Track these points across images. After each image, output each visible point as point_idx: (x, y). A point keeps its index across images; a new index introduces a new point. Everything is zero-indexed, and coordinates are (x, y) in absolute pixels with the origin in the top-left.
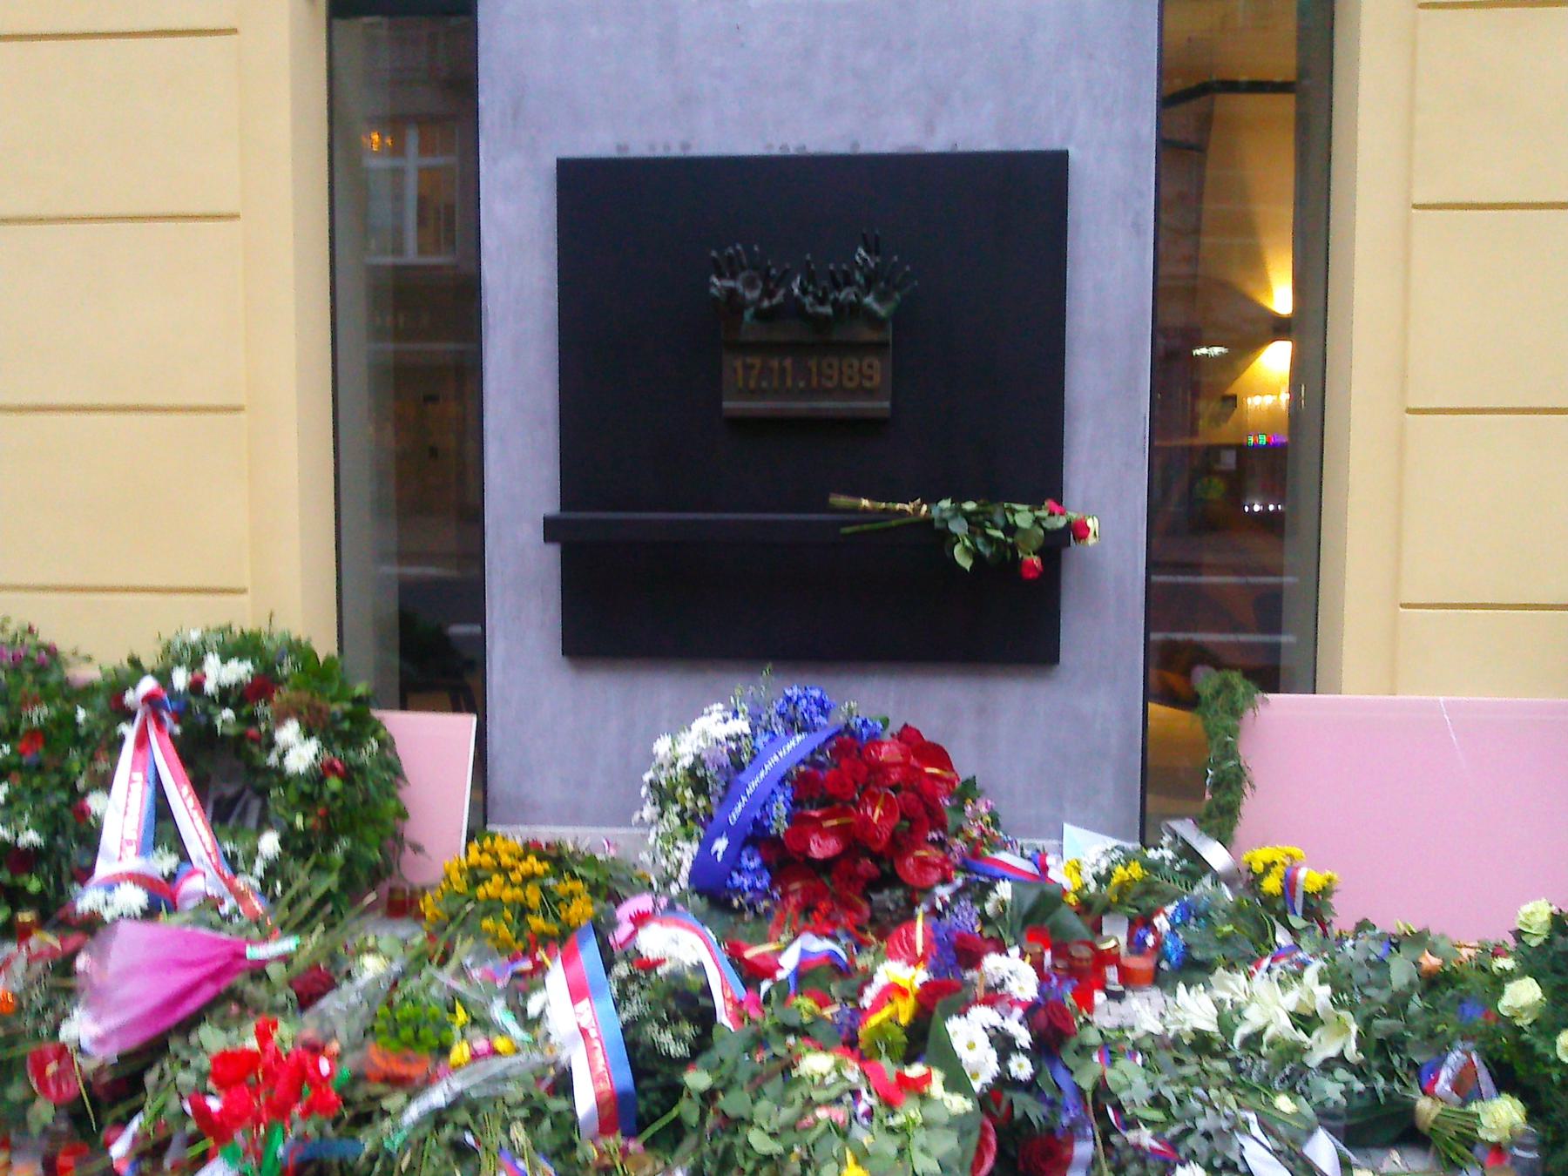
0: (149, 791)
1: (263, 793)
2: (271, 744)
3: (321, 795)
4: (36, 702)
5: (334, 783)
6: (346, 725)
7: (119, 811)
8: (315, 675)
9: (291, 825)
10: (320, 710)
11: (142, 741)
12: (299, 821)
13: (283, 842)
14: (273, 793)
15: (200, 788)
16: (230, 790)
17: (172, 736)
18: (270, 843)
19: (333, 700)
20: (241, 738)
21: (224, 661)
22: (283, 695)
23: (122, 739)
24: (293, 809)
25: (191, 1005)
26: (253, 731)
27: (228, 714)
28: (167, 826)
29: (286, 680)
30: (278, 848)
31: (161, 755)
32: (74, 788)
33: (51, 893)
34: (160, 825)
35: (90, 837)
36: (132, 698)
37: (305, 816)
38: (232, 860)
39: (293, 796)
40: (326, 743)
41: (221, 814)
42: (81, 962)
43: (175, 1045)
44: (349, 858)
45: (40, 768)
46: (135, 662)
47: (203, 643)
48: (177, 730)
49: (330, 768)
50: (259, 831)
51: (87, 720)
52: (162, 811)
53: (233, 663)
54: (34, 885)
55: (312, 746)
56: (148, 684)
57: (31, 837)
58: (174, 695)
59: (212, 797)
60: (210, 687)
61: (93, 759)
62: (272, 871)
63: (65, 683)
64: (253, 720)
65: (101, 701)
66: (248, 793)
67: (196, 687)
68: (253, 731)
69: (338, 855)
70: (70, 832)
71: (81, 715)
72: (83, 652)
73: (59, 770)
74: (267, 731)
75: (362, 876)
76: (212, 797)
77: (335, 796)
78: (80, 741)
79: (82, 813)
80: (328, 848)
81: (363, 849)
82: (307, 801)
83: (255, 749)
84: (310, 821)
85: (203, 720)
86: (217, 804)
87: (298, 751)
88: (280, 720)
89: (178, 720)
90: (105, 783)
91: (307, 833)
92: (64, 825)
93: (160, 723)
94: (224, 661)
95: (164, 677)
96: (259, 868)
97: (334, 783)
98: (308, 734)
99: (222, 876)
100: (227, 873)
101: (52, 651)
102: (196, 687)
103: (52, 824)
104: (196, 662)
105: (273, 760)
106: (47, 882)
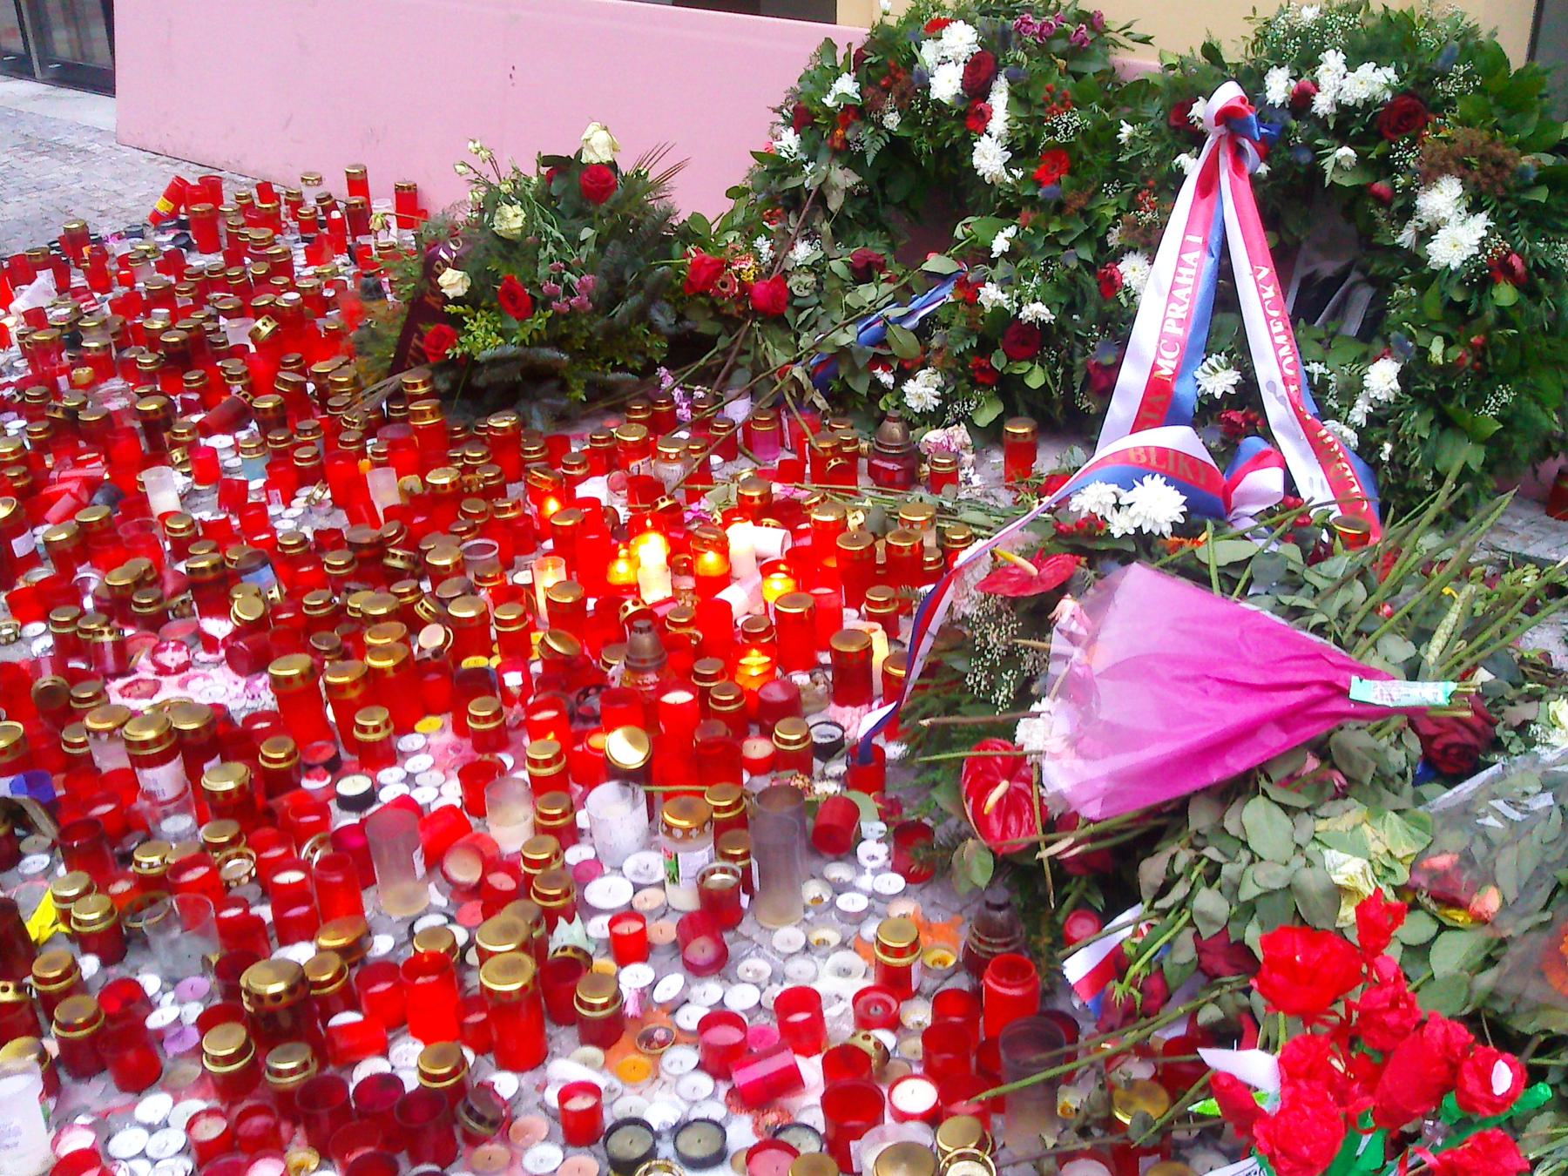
0: (1209, 263)
1: (1383, 286)
2: (1408, 212)
3: (1479, 313)
4: (1066, 104)
5: (1505, 294)
6: (1541, 195)
7: (1161, 291)
8: (1499, 99)
9: (1424, 352)
10: (1500, 165)
11: (1208, 184)
12: (1437, 349)
13: (1403, 377)
14: (1400, 292)
15: (1283, 259)
16: (1328, 268)
17: (1254, 180)
18: (1383, 378)
19: (1524, 147)
20: (1359, 191)
21: (1351, 66)
22: (1445, 130)
23: (1179, 177)
24: (1430, 328)
25: (1236, 763)
26: (1382, 186)
27: (1346, 152)
28: (1227, 319)
29: (1449, 102)
30: (1396, 386)
31: (1234, 209)
32: (1102, 245)
33: (1056, 392)
34: (1219, 317)
35: (1117, 322)
36: (1203, 111)
37: (1449, 342)
38: (1318, 389)
39: (1433, 307)
40: (1503, 224)
41: (1308, 306)
42: (1067, 607)
43: (1200, 818)
44: (1508, 420)
45: (1060, 208)
46: (1211, 52)
47: (1321, 25)
48: (1263, 169)
49: (1502, 268)
50: (1368, 359)
51: (1132, 138)
52: (1224, 297)
53: (1366, 69)
54: (1036, 379)
55: (1479, 224)
56: (1229, 93)
57: (1036, 311)
58: (1266, 112)
59: (1301, 271)
60: (1322, 104)
61: (1134, 205)
62: (1381, 417)
63: (1110, 73)
64: (1385, 167)
65: (1154, 109)
66: (1354, 276)
67: (1301, 102)
68: (1382, 186)
69: (1488, 418)
70: (1091, 309)
71: (1126, 130)
72: (1137, 30)
73: (1085, 214)
74: (1405, 188)
75: (1523, 449)
76: (1301, 271)
77: (1504, 318)
78: (1117, 172)
79: (1111, 284)
80: (1476, 401)
81: (1533, 408)
82: (1458, 317)
83: (1380, 214)
84: (1456, 353)
85: (1305, 157)
86: (1306, 282)
87: (1454, 230)
88: (1429, 178)
89: (1264, 157)
90: (1149, 243)
91: (1446, 370)
92: (1084, 301)
93: (1238, 154)
94: (1351, 66)
95: (1252, 79)
96: (1359, 414)
97: (1505, 294)
98: (1474, 208)
99: (1300, 416)
100: (1310, 409)
101: (1093, 21)
102: (1301, 102)
103: (1069, 297)
104: (1307, 62)
105: (1406, 237)
106: (1054, 377)
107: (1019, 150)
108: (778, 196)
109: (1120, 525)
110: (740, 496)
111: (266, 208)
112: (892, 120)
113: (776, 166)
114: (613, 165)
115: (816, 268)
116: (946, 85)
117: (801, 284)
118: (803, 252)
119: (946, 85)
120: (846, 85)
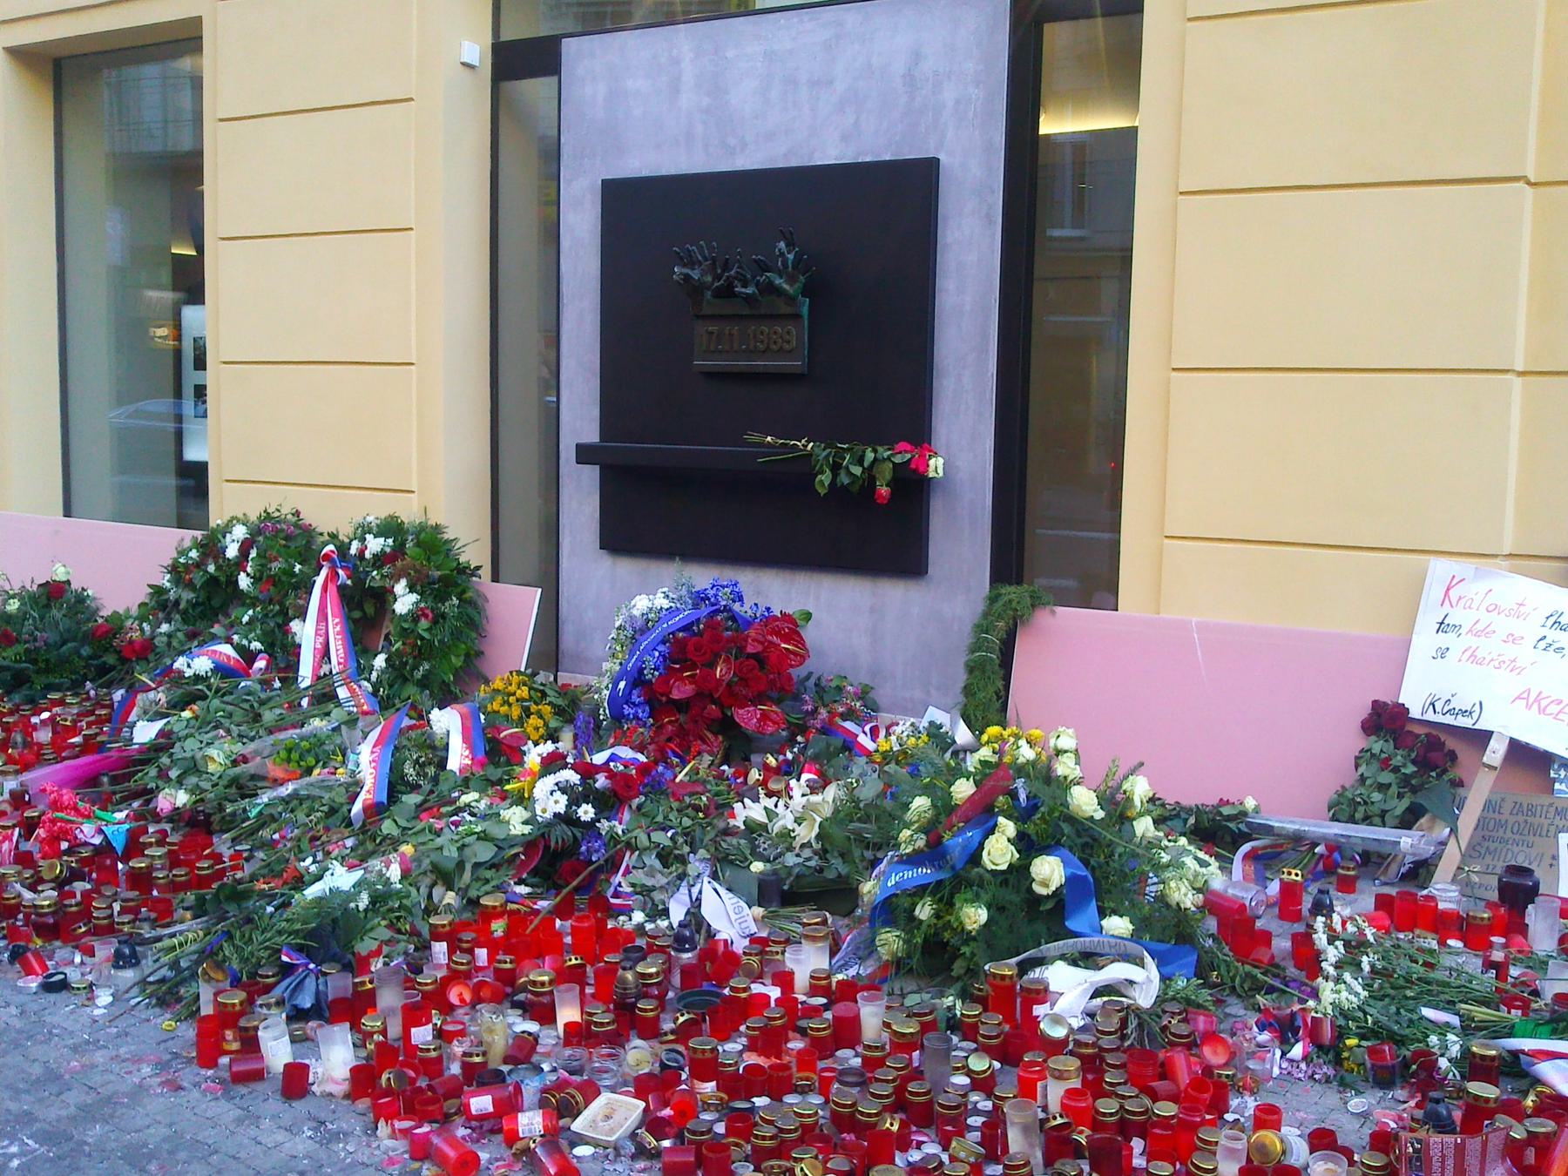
55: (414, 597)
60: (368, 555)
67: (362, 552)
107: (256, 579)
108: (160, 604)
109: (189, 673)
110: (217, 1004)
111: (986, 615)
112: (211, 568)
113: (158, 591)
114: (68, 582)
115: (170, 636)
116: (232, 552)
117: (160, 642)
118: (165, 628)
119: (232, 552)
120: (194, 554)
